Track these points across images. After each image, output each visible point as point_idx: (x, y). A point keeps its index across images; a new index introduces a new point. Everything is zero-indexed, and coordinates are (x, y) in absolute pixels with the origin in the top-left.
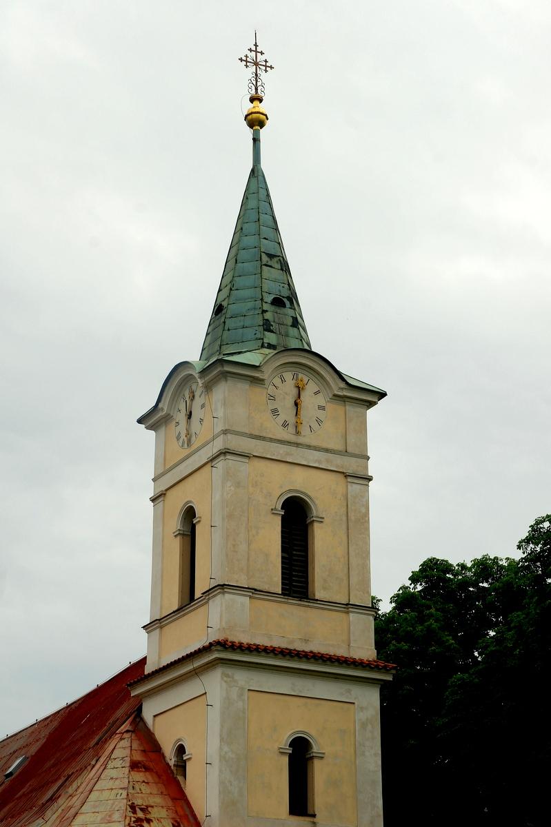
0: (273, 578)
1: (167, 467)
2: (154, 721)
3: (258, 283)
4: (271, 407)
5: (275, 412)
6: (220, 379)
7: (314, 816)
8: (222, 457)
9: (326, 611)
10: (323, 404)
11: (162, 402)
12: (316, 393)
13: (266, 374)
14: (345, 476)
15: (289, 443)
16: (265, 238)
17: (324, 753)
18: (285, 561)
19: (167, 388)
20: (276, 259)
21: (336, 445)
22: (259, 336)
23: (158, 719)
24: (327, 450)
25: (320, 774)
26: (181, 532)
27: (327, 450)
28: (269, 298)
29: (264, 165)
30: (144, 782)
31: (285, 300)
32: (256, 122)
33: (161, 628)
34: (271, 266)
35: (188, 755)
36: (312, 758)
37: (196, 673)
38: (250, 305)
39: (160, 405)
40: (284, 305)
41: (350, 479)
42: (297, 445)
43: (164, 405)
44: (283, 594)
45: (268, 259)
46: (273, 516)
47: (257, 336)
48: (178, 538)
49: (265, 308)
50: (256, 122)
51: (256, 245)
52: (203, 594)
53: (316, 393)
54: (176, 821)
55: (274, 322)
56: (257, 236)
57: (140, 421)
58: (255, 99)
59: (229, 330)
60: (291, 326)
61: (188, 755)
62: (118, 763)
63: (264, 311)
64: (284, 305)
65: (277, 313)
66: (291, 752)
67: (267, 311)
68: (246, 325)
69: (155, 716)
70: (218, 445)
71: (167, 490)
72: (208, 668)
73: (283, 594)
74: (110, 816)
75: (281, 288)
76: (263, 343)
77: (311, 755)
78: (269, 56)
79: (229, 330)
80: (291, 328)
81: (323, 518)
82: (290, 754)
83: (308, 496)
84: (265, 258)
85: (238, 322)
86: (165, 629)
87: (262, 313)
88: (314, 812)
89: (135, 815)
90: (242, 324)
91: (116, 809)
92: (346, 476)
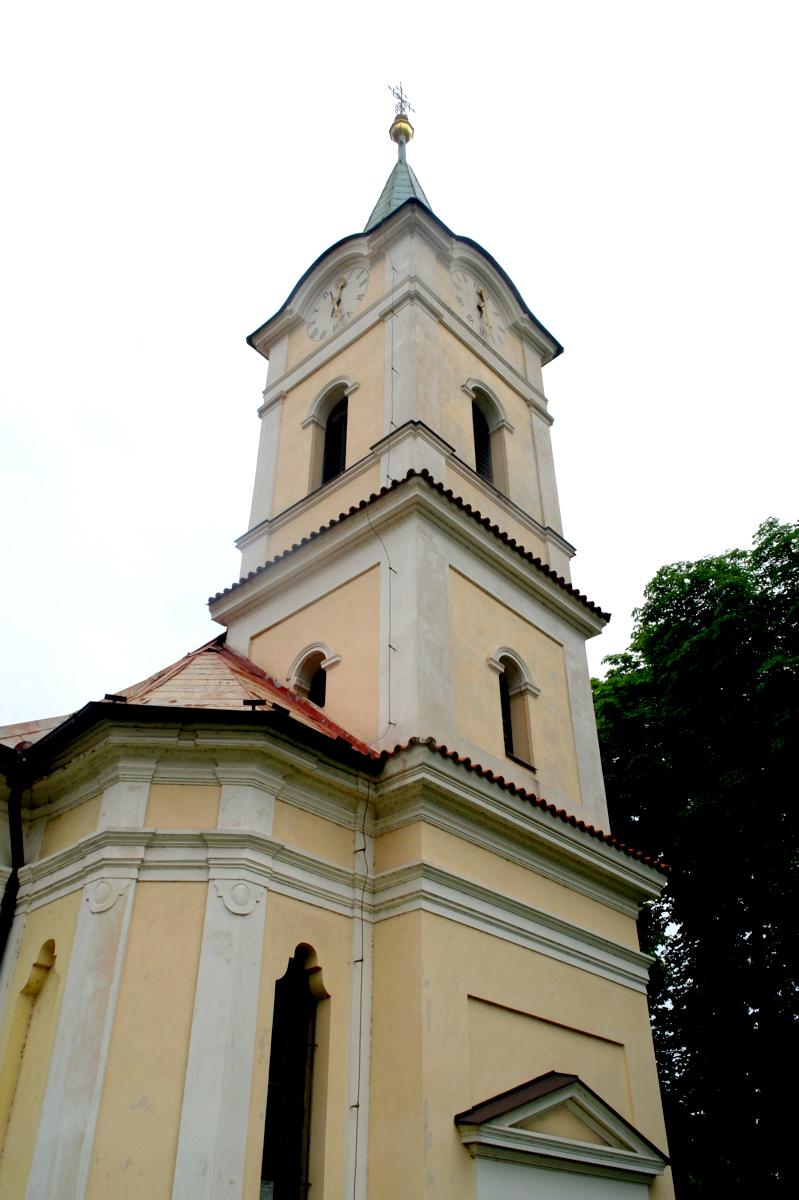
1: (290, 368)
2: (251, 645)
6: (404, 234)
8: (408, 301)
11: (292, 304)
13: (453, 264)
14: (528, 405)
17: (539, 691)
19: (307, 281)
23: (256, 641)
26: (316, 420)
29: (409, 160)
32: (400, 135)
33: (270, 533)
35: (330, 659)
36: (522, 693)
37: (376, 532)
39: (288, 308)
43: (295, 306)
46: (462, 394)
48: (311, 427)
50: (400, 135)
52: (372, 448)
57: (250, 340)
58: (401, 118)
61: (330, 659)
69: (252, 638)
70: (407, 288)
71: (288, 392)
72: (389, 526)
77: (523, 688)
83: (490, 390)
86: (275, 535)
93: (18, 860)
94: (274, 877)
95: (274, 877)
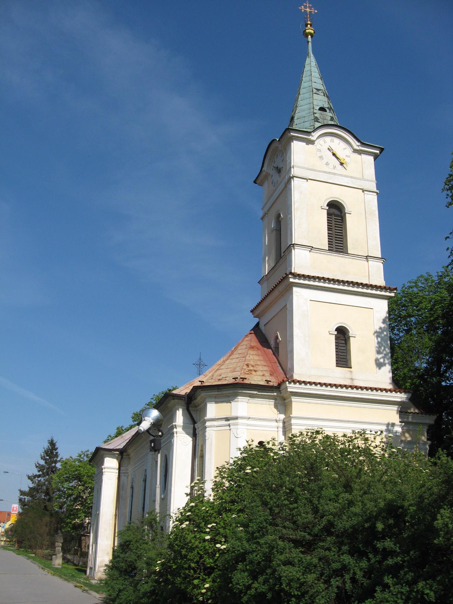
0: (324, 243)
3: (311, 101)
4: (319, 155)
5: (321, 157)
7: (351, 368)
9: (354, 260)
10: (349, 155)
12: (344, 149)
15: (330, 173)
16: (314, 82)
18: (329, 235)
20: (321, 91)
21: (360, 176)
22: (312, 124)
24: (352, 177)
25: (354, 345)
27: (352, 177)
28: (318, 108)
30: (256, 355)
31: (326, 109)
34: (318, 94)
38: (307, 112)
40: (326, 111)
41: (365, 192)
42: (335, 174)
44: (329, 250)
45: (316, 91)
47: (311, 125)
49: (315, 112)
51: (310, 85)
53: (344, 149)
54: (272, 372)
55: (320, 118)
56: (311, 82)
59: (296, 125)
60: (330, 120)
62: (244, 347)
63: (314, 113)
64: (326, 111)
65: (322, 114)
66: (336, 333)
67: (316, 113)
68: (305, 120)
69: (265, 325)
73: (329, 250)
74: (234, 369)
75: (324, 104)
76: (314, 127)
78: (248, 440)
79: (296, 125)
80: (330, 121)
81: (351, 212)
82: (336, 335)
84: (315, 91)
85: (302, 120)
87: (314, 114)
88: (351, 366)
89: (248, 368)
90: (303, 121)
91: (238, 366)
92: (363, 191)
93: (194, 422)
94: (248, 425)
95: (248, 425)
